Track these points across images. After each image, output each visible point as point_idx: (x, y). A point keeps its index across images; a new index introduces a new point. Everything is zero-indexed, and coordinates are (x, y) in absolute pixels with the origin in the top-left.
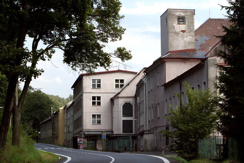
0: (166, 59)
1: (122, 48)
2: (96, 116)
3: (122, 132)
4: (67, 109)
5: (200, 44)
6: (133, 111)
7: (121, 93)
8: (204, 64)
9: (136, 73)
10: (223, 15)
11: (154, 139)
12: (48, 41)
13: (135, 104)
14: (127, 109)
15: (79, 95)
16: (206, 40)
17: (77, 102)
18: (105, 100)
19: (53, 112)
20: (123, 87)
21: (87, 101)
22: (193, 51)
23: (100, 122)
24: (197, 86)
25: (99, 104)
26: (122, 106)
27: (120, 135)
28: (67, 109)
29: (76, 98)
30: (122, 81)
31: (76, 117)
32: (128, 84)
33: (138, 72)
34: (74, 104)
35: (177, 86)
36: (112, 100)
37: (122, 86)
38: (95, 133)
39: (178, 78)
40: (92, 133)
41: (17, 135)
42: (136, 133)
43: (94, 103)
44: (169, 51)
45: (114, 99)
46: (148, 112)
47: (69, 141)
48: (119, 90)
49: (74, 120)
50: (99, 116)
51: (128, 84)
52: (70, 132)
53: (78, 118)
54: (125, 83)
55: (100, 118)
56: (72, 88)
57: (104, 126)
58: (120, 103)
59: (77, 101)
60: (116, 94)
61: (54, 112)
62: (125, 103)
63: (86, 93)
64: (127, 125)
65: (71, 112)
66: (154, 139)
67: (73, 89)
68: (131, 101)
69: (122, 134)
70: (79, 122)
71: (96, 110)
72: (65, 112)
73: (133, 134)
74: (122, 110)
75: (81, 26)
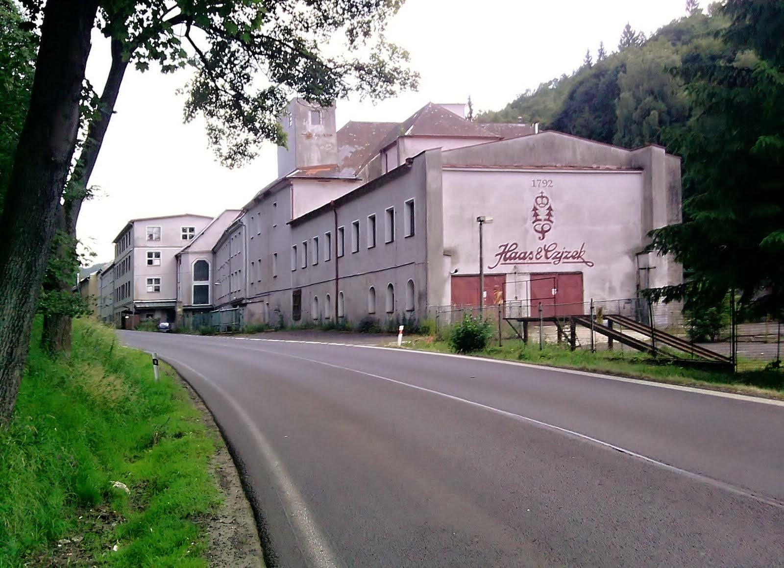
0: (294, 180)
2: (154, 280)
4: (103, 275)
8: (411, 168)
11: (264, 310)
14: (202, 269)
15: (127, 250)
16: (351, 152)
17: (120, 263)
18: (167, 256)
19: (80, 280)
20: (194, 239)
22: (334, 168)
24: (368, 219)
26: (193, 264)
28: (103, 275)
30: (192, 230)
31: (119, 283)
33: (216, 216)
34: (116, 266)
35: (330, 217)
36: (178, 257)
38: (152, 305)
39: (332, 204)
41: (748, 17)
44: (297, 167)
45: (180, 256)
46: (250, 270)
48: (187, 243)
50: (157, 281)
54: (196, 232)
55: (159, 283)
56: (114, 242)
57: (162, 298)
58: (191, 261)
59: (123, 260)
61: (82, 280)
64: (201, 292)
65: (109, 277)
66: (264, 310)
70: (126, 289)
71: (153, 273)
72: (99, 279)
73: (209, 304)
74: (193, 271)
75: (277, 41)
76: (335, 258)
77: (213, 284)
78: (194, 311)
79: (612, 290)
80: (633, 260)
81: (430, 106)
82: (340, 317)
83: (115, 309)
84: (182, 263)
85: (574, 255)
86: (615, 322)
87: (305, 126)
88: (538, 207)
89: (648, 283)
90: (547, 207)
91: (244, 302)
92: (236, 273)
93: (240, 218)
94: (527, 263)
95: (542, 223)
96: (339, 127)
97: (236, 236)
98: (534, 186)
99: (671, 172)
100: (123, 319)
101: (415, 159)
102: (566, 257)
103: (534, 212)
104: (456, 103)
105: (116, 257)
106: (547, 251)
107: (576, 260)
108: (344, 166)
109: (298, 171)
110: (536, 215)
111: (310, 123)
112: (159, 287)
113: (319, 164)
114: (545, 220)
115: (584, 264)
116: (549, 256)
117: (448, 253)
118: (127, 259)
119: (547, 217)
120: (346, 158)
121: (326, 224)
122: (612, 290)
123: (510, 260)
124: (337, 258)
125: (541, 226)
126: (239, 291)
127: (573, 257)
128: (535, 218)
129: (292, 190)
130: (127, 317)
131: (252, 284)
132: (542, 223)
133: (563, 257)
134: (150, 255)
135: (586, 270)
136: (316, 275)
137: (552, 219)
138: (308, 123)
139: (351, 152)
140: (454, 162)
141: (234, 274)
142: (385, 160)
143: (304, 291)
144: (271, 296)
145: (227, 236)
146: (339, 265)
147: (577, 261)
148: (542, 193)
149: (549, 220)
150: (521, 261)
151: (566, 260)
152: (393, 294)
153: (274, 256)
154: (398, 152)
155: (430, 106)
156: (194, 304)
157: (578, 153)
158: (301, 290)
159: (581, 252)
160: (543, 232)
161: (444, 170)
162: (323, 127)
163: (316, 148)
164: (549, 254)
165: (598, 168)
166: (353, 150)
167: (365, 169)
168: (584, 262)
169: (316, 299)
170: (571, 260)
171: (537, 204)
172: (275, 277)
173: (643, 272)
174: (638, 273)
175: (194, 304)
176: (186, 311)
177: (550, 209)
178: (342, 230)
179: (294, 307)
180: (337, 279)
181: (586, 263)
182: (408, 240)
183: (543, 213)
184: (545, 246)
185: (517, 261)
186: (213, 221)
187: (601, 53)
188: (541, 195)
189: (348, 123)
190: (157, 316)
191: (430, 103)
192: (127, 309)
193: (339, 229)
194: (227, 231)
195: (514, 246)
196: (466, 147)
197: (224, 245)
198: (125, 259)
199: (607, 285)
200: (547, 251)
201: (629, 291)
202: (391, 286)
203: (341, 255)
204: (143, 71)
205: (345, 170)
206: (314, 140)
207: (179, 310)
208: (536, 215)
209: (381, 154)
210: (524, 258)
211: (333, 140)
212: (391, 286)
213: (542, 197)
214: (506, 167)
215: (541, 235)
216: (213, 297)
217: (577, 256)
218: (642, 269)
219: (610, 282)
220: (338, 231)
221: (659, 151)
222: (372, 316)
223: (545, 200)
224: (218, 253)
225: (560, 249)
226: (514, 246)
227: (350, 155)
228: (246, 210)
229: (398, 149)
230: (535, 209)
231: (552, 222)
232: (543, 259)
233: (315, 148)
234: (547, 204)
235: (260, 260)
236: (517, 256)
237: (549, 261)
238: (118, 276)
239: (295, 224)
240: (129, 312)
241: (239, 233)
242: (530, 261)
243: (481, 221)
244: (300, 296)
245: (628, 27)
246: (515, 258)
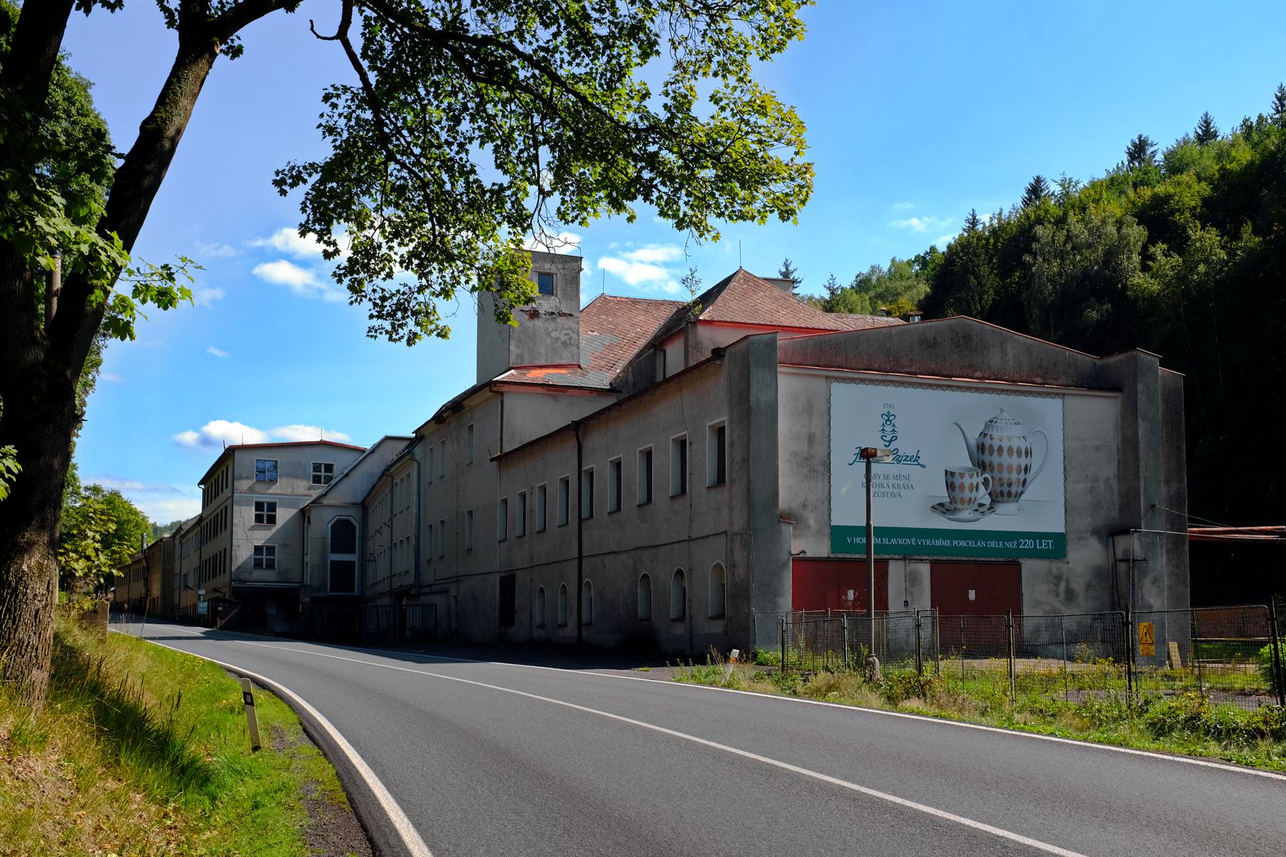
1: (206, 304)
2: (264, 566)
4: (183, 536)
6: (357, 539)
7: (329, 495)
9: (363, 451)
12: (403, 318)
17: (212, 517)
20: (333, 482)
21: (244, 515)
25: (272, 520)
26: (330, 525)
29: (213, 504)
30: (329, 468)
32: (347, 475)
34: (204, 523)
37: (329, 479)
43: (259, 519)
47: (186, 575)
49: (203, 559)
51: (347, 475)
55: (274, 555)
56: (199, 484)
59: (215, 514)
62: (338, 520)
67: (203, 486)
68: (353, 516)
70: (223, 557)
71: (262, 537)
76: (577, 520)
77: (364, 560)
79: (1070, 596)
82: (585, 624)
84: (312, 522)
92: (401, 541)
97: (402, 480)
109: (513, 371)
118: (222, 511)
122: (1070, 596)
124: (580, 521)
129: (502, 402)
130: (220, 609)
141: (398, 544)
142: (662, 356)
143: (519, 576)
146: (585, 534)
152: (684, 588)
158: (514, 575)
169: (542, 590)
173: (1122, 567)
175: (330, 591)
178: (591, 474)
180: (580, 557)
182: (713, 492)
186: (365, 454)
193: (585, 471)
196: (322, 444)
198: (219, 511)
199: (1063, 586)
204: (281, 195)
209: (655, 350)
218: (1121, 561)
219: (1068, 582)
220: (583, 474)
221: (1148, 358)
229: (686, 341)
235: (442, 522)
239: (504, 459)
245: (1206, 115)
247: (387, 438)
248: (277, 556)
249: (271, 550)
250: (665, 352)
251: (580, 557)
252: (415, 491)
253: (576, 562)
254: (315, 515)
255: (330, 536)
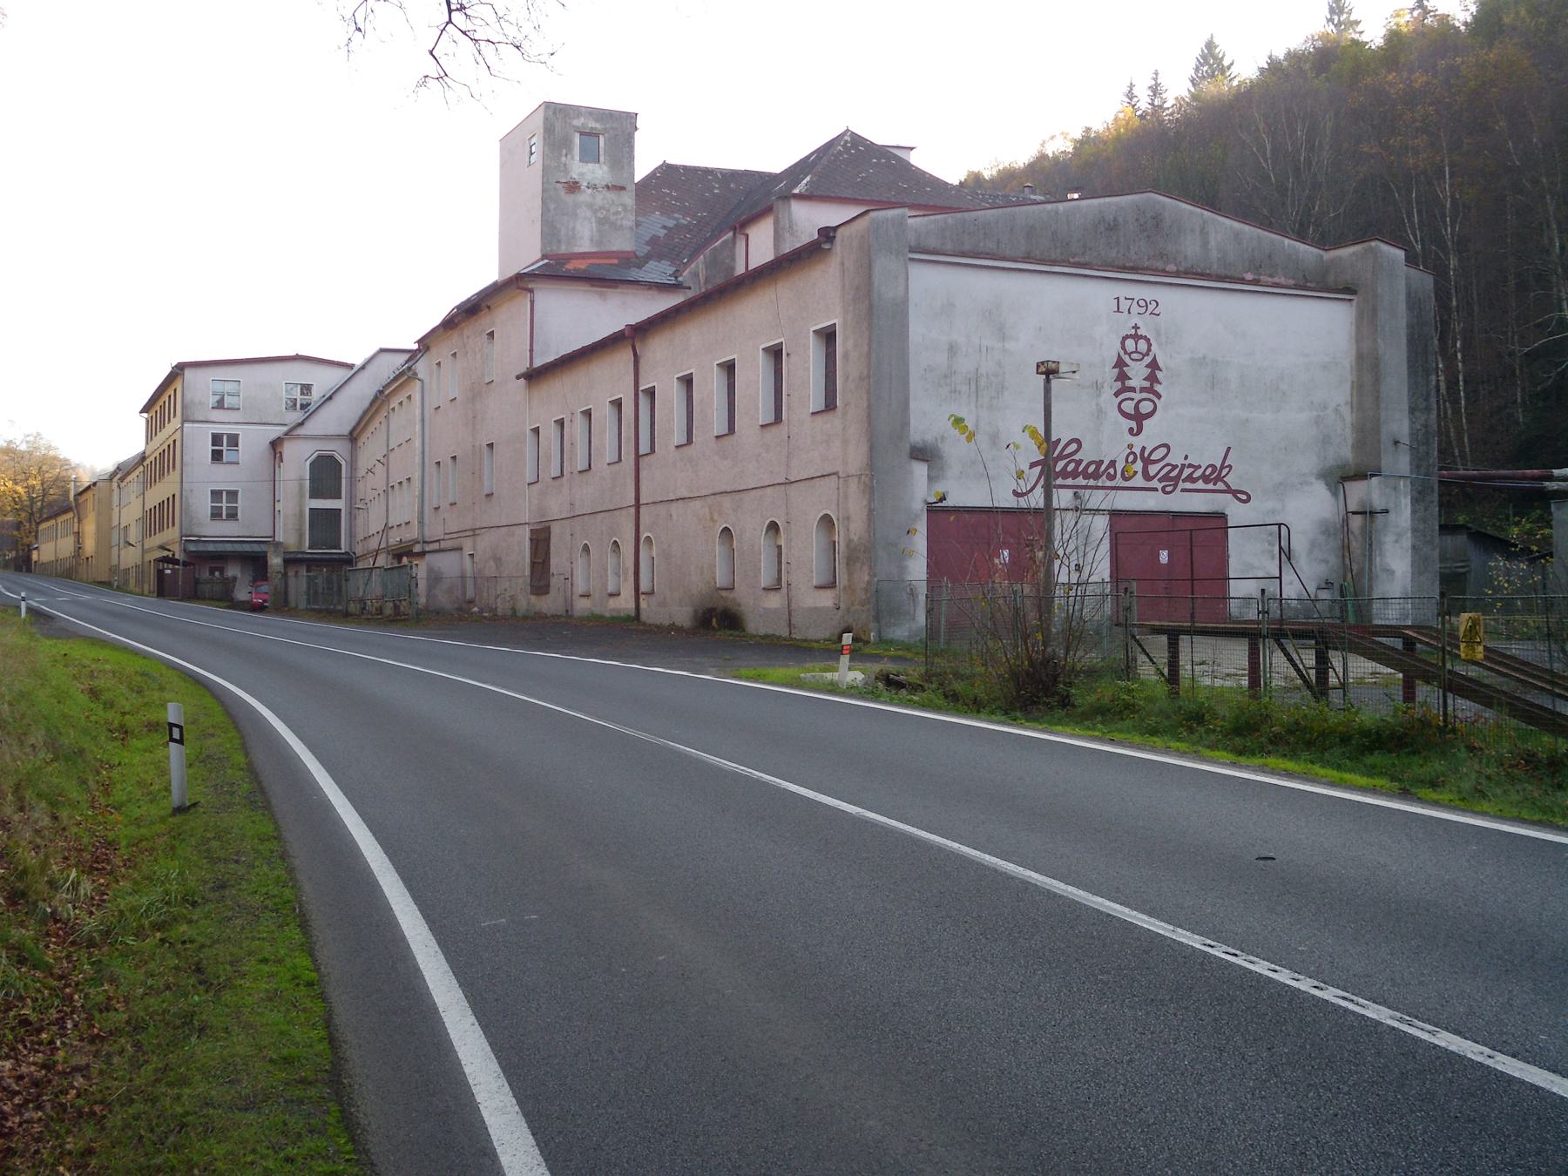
2: (224, 493)
3: (307, 545)
5: (647, 239)
6: (343, 481)
9: (351, 366)
10: (98, 470)
13: (348, 459)
16: (664, 227)
18: (253, 441)
23: (237, 514)
26: (308, 463)
27: (300, 556)
30: (306, 389)
32: (330, 398)
34: (148, 462)
35: (623, 358)
36: (275, 445)
38: (220, 548)
40: (211, 548)
42: (351, 549)
49: (147, 508)
51: (330, 398)
52: (130, 544)
53: (161, 501)
56: (145, 409)
59: (161, 450)
60: (690, 294)
63: (193, 422)
64: (325, 523)
69: (309, 551)
71: (222, 477)
73: (343, 551)
78: (311, 563)
80: (1335, 494)
81: (847, 138)
83: (144, 552)
85: (1207, 473)
86: (1421, 642)
87: (565, 165)
88: (1126, 359)
89: (1371, 545)
90: (1148, 360)
91: (417, 549)
92: (400, 483)
93: (410, 363)
94: (1103, 488)
95: (1137, 396)
96: (641, 170)
97: (401, 403)
98: (1118, 311)
99: (1414, 303)
100: (160, 573)
101: (840, 231)
102: (1190, 479)
103: (1116, 370)
104: (895, 144)
105: (147, 443)
106: (1147, 462)
107: (1210, 486)
108: (648, 257)
110: (1123, 377)
111: (577, 158)
112: (236, 507)
113: (594, 250)
114: (1143, 390)
115: (1229, 496)
116: (1152, 473)
117: (922, 453)
119: (1147, 384)
120: (654, 241)
121: (611, 377)
123: (1065, 478)
124: (638, 457)
125: (1135, 401)
126: (407, 523)
127: (1206, 479)
128: (1119, 383)
131: (437, 509)
132: (1137, 396)
133: (1184, 476)
134: (217, 439)
135: (1236, 512)
136: (587, 494)
137: (1158, 388)
138: (573, 158)
139: (664, 227)
140: (932, 243)
141: (397, 486)
143: (556, 530)
144: (479, 538)
145: (380, 400)
146: (643, 474)
147: (1214, 488)
148: (1136, 327)
149: (1151, 390)
150: (1092, 482)
151: (1188, 485)
153: (485, 449)
154: (776, 231)
155: (847, 138)
156: (309, 548)
157: (1213, 243)
159: (1222, 467)
160: (1139, 418)
161: (912, 260)
162: (605, 168)
163: (589, 214)
164: (1153, 470)
165: (1256, 282)
166: (671, 223)
167: (697, 266)
168: (1229, 490)
169: (586, 548)
170: (1200, 485)
171: (1126, 352)
172: (489, 495)
174: (1346, 521)
176: (291, 561)
177: (1154, 365)
178: (651, 393)
179: (533, 564)
180: (638, 505)
181: (1235, 493)
182: (819, 418)
183: (1137, 373)
184: (1144, 449)
185: (1081, 481)
186: (353, 372)
187: (1155, 90)
188: (1133, 332)
189: (660, 167)
190: (233, 571)
191: (848, 130)
192: (170, 554)
194: (381, 392)
195: (1074, 447)
197: (376, 423)
200: (1147, 462)
201: (1327, 562)
202: (773, 527)
203: (648, 451)
205: (652, 264)
206: (585, 196)
207: (275, 561)
208: (1123, 377)
210: (1096, 475)
211: (628, 199)
212: (773, 527)
213: (1137, 337)
214: (1054, 263)
215: (1133, 424)
216: (352, 535)
217: (1215, 476)
218: (1354, 513)
220: (640, 393)
222: (724, 594)
223: (1142, 346)
224: (363, 439)
225: (1176, 458)
226: (1074, 447)
227: (662, 233)
228: (425, 343)
230: (1120, 364)
231: (1159, 396)
232: (1139, 481)
233: (584, 212)
234: (1147, 354)
235: (454, 458)
236: (1080, 469)
237: (1155, 483)
238: (149, 481)
240: (173, 561)
241: (409, 397)
242: (1109, 484)
243: (1049, 371)
244: (548, 540)
245: (1210, 45)
246: (1075, 474)
247: (382, 351)
248: (240, 504)
249: (233, 495)
250: (748, 235)
251: (638, 505)
252: (418, 418)
253: (633, 510)
254: (288, 449)
255: (308, 477)
